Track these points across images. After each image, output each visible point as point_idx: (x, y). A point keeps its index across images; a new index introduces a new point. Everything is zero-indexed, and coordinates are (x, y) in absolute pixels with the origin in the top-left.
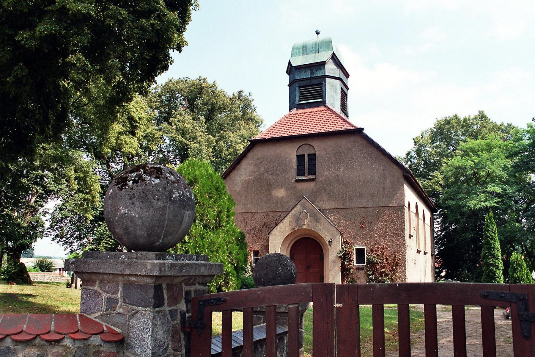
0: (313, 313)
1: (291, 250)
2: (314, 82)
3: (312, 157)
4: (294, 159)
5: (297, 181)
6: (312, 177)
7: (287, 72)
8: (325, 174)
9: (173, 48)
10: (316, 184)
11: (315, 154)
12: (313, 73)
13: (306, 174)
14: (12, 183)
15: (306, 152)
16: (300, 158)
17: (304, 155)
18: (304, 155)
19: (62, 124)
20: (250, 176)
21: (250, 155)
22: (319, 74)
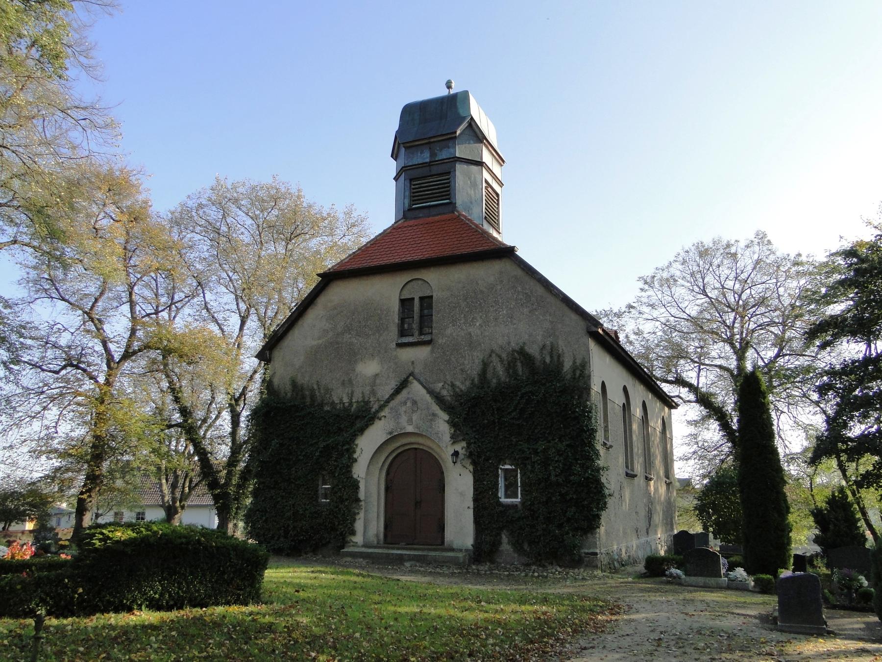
0: (626, 352)
1: (388, 473)
2: (435, 170)
3: (427, 301)
4: (395, 306)
5: (400, 345)
6: (427, 338)
7: (392, 156)
8: (448, 332)
9: (693, 488)
10: (432, 351)
11: (432, 297)
12: (436, 155)
13: (416, 333)
14: (841, 417)
15: (416, 293)
16: (405, 303)
17: (413, 299)
18: (413, 299)
19: (494, 381)
20: (319, 338)
21: (322, 300)
22: (444, 155)
